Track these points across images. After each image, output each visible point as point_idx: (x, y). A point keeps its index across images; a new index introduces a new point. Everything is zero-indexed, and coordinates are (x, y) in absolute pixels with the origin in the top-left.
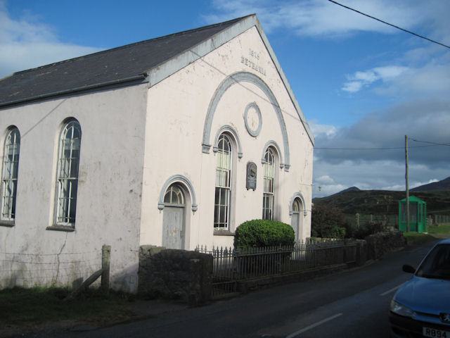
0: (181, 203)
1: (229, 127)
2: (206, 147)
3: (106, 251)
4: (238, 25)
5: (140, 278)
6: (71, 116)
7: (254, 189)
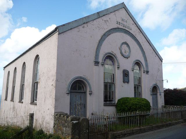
1: (110, 53)
2: (97, 63)
7: (128, 82)
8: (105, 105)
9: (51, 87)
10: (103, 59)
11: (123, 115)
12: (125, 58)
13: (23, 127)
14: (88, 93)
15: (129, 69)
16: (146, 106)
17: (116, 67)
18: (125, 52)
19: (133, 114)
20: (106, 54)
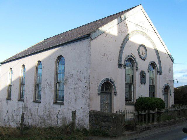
0: (109, 91)
1: (131, 56)
2: (120, 66)
3: (74, 113)
4: (133, 9)
5: (90, 125)
6: (61, 55)
7: (144, 83)
8: (127, 104)
9: (84, 88)
10: (125, 62)
11: (142, 113)
12: (142, 60)
13: (14, 126)
14: (113, 93)
15: (146, 71)
16: (161, 104)
17: (135, 68)
18: (143, 54)
19: (153, 112)
20: (127, 57)
